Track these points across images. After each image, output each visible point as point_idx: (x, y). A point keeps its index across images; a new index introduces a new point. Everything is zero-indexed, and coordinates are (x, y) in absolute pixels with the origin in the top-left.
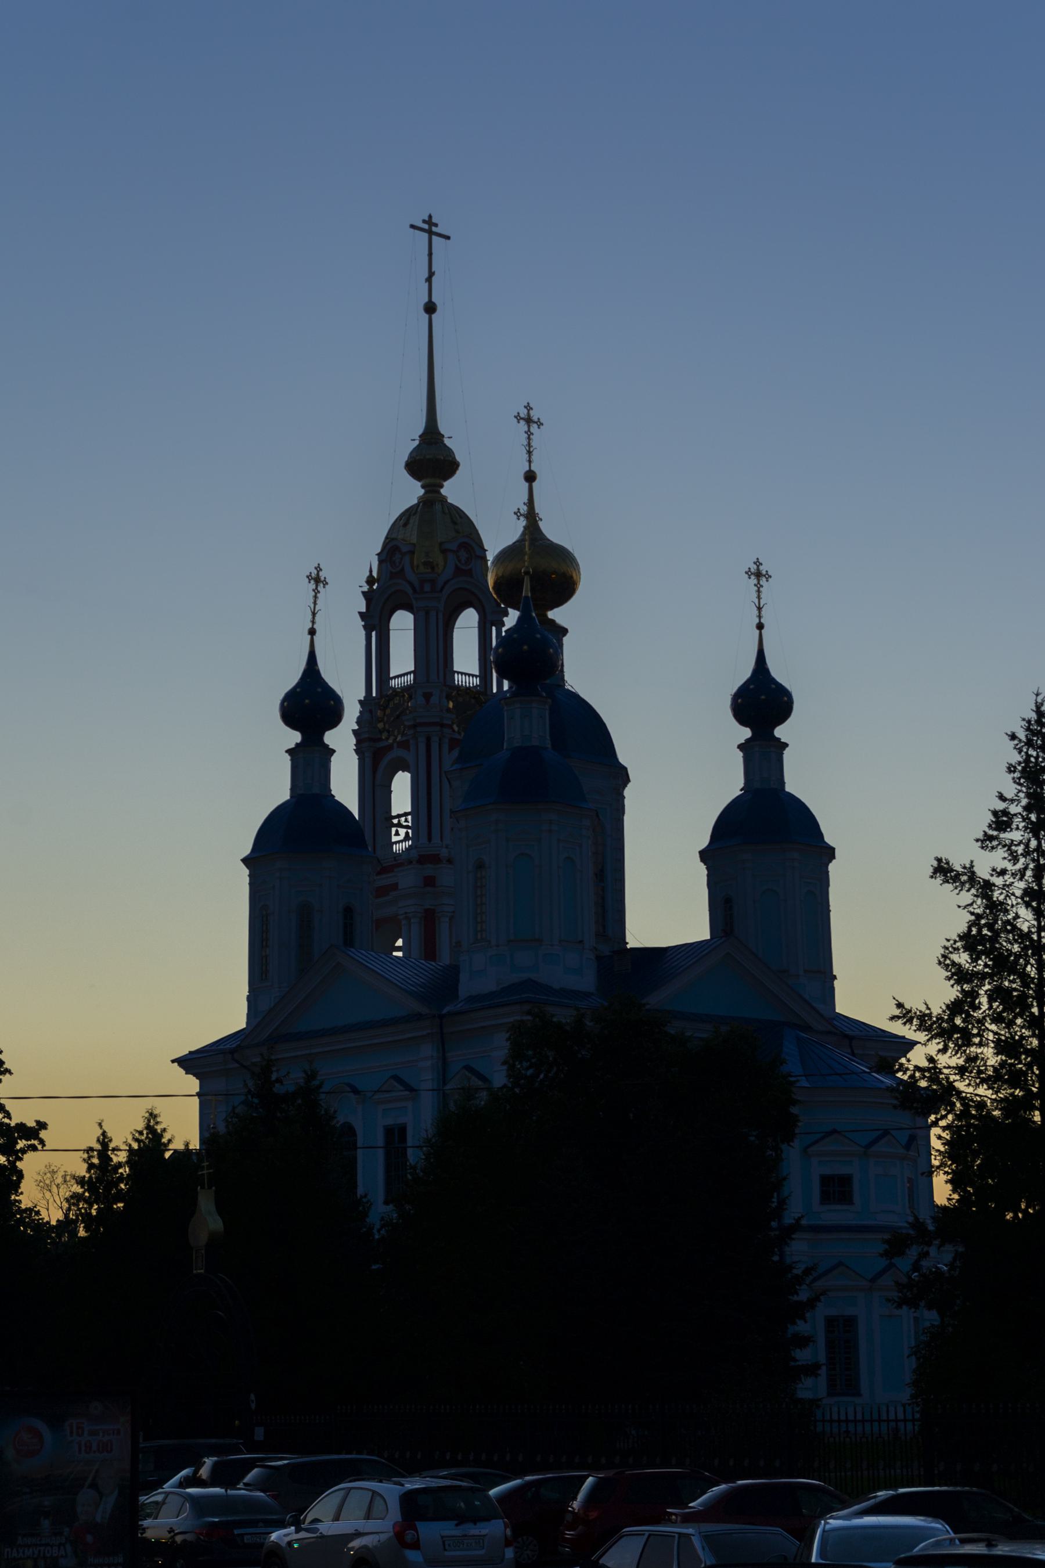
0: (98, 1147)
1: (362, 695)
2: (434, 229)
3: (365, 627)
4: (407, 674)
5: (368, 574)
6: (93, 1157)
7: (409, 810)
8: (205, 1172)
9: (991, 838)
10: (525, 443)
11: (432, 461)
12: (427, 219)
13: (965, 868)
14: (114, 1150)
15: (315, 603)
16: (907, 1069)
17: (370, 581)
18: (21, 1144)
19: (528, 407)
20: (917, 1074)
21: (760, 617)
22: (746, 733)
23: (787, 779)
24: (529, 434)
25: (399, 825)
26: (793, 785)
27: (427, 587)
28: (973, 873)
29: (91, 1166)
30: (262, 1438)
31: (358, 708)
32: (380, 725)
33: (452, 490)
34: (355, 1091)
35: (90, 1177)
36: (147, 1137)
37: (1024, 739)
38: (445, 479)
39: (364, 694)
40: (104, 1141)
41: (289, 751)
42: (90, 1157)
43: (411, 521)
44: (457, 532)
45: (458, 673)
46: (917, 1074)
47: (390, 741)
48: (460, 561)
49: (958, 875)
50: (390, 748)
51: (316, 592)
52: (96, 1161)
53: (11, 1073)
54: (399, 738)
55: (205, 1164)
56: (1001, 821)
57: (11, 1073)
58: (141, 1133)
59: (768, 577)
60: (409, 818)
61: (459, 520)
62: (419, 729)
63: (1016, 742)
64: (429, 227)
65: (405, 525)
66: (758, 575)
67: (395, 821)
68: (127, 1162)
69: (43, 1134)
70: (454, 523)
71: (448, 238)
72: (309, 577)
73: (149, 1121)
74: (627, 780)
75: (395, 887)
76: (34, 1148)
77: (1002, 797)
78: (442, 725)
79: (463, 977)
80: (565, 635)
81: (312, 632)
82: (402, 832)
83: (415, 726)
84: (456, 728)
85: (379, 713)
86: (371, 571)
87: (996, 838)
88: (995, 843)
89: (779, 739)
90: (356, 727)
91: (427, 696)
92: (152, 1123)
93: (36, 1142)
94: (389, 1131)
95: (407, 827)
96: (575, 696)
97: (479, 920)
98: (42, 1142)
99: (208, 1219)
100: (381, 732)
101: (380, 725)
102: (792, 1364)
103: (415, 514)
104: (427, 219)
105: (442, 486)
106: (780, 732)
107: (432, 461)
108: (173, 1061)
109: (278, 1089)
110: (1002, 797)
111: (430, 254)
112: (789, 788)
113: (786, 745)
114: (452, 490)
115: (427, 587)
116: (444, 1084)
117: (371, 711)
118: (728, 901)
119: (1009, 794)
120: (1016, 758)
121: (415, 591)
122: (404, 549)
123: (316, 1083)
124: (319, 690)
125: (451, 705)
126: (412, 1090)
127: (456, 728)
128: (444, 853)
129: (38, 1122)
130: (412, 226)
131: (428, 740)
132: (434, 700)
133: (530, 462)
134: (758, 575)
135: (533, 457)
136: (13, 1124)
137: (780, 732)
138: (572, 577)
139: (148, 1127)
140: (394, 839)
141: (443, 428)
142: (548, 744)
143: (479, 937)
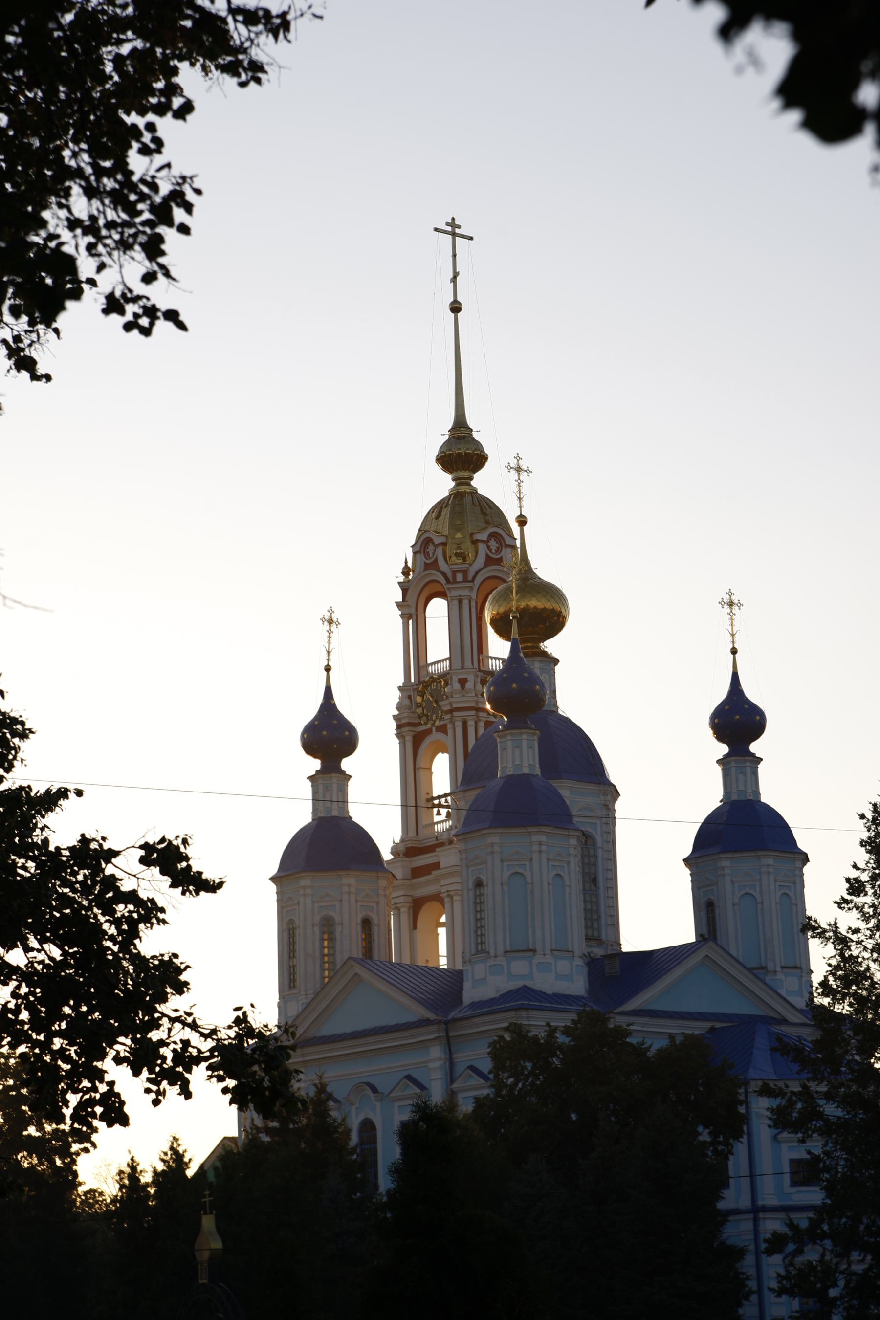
1: (401, 681)
2: (457, 231)
3: (402, 616)
4: (443, 661)
5: (403, 565)
7: (448, 791)
8: (207, 1199)
9: (847, 902)
10: (516, 490)
12: (450, 221)
13: (830, 925)
14: (141, 1171)
16: (785, 1094)
17: (406, 572)
18: (75, 1147)
19: (518, 458)
20: (794, 1098)
22: (724, 749)
23: (762, 790)
24: (519, 482)
25: (440, 806)
27: (459, 577)
28: (837, 928)
32: (419, 711)
33: (483, 482)
34: (374, 1089)
35: (122, 1197)
36: (171, 1158)
37: (870, 818)
38: (475, 472)
39: (403, 681)
40: (133, 1166)
43: (443, 513)
44: (487, 522)
45: (492, 658)
46: (794, 1098)
47: (429, 726)
48: (490, 550)
49: (825, 931)
50: (428, 732)
51: (330, 632)
54: (437, 723)
55: (207, 1193)
56: (856, 887)
60: (449, 798)
61: (488, 511)
62: (455, 714)
63: (865, 821)
64: (453, 230)
65: (437, 518)
67: (436, 802)
68: (153, 1182)
70: (485, 514)
71: (471, 238)
72: (323, 620)
75: (436, 866)
76: (86, 1150)
77: (855, 866)
79: (467, 985)
80: (556, 664)
81: (328, 669)
83: (451, 711)
85: (419, 699)
86: (406, 562)
87: (851, 901)
88: (851, 906)
89: (753, 755)
90: (396, 713)
91: (463, 682)
93: (88, 1145)
96: (567, 721)
97: (479, 933)
98: (94, 1145)
99: (210, 1238)
100: (420, 717)
101: (419, 711)
103: (446, 507)
104: (450, 221)
105: (472, 479)
110: (855, 866)
111: (454, 256)
112: (764, 799)
114: (483, 482)
115: (459, 577)
116: (452, 1082)
117: (410, 697)
119: (862, 865)
120: (865, 835)
121: (448, 581)
122: (437, 540)
124: (335, 722)
130: (436, 230)
131: (465, 723)
132: (469, 685)
133: (520, 507)
135: (523, 503)
138: (561, 612)
139: (172, 1148)
140: (436, 819)
141: (471, 422)
142: (538, 771)
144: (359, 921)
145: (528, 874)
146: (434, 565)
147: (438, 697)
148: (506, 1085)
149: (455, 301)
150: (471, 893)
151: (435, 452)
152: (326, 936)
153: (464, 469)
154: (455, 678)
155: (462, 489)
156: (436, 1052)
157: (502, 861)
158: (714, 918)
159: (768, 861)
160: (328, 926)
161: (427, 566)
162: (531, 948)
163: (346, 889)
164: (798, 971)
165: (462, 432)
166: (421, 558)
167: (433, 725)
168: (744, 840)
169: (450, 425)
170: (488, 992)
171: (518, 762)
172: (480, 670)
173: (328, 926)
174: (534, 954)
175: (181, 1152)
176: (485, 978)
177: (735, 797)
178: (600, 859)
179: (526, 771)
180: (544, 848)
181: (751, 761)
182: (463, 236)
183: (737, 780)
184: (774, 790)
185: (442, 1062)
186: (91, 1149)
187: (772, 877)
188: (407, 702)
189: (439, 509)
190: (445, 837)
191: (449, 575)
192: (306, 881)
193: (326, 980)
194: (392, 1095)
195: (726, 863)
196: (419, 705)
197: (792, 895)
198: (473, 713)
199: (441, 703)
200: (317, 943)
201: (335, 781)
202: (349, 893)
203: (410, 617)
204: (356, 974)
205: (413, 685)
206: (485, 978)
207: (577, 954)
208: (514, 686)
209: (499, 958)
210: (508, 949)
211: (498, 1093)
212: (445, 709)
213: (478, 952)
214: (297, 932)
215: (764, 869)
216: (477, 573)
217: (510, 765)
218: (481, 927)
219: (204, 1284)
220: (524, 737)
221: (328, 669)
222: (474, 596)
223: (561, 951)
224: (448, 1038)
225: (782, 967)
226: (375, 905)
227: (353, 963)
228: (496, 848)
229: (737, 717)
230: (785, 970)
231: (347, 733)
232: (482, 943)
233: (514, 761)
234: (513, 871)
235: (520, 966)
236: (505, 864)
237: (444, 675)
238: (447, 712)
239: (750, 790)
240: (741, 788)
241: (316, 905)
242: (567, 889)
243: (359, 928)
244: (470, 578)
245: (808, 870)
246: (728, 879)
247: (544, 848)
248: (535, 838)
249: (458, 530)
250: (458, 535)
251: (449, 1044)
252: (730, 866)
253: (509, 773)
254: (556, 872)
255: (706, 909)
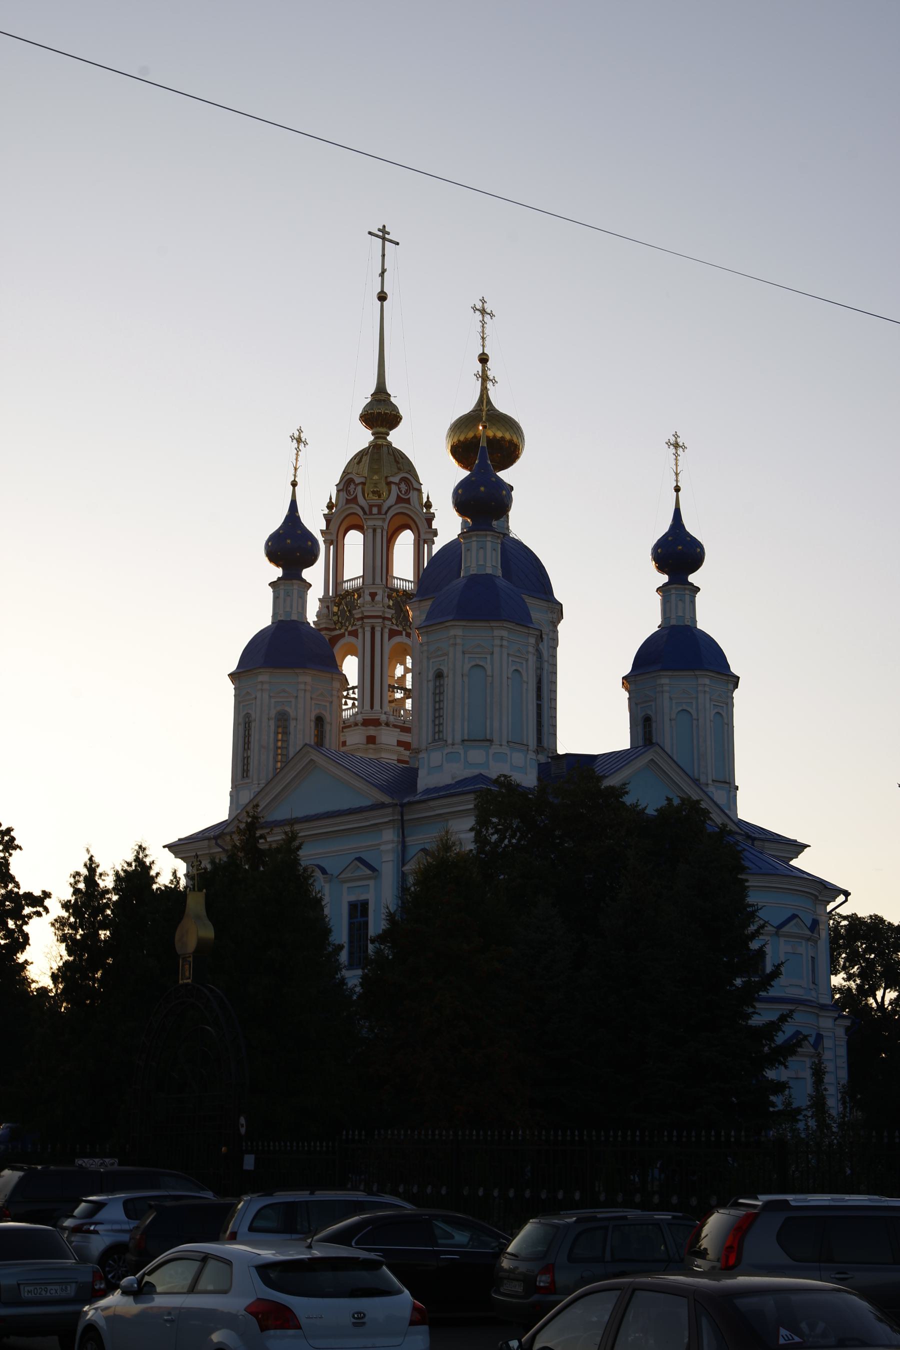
0: (84, 872)
2: (387, 236)
4: (357, 578)
6: (79, 881)
7: (356, 684)
10: (480, 330)
11: (381, 414)
14: (101, 875)
15: (297, 460)
17: (330, 506)
18: (27, 910)
19: (483, 301)
21: (677, 481)
24: (483, 323)
26: (703, 624)
27: (375, 510)
29: (76, 891)
30: (252, 1168)
31: (318, 604)
32: (335, 618)
33: (397, 438)
38: (391, 430)
40: (92, 866)
41: (272, 584)
42: (76, 882)
44: (399, 469)
45: (397, 578)
47: (343, 631)
48: (401, 492)
50: (343, 635)
51: (298, 450)
52: (82, 886)
53: (21, 848)
57: (21, 848)
58: (129, 864)
59: (684, 448)
60: (356, 690)
61: (401, 462)
62: (365, 621)
64: (383, 235)
65: (359, 463)
66: (676, 445)
69: (47, 902)
70: (398, 462)
71: (398, 244)
73: (138, 853)
74: (560, 616)
76: (39, 914)
78: (384, 618)
79: (422, 773)
81: (294, 484)
82: (350, 702)
83: (362, 619)
84: (394, 622)
85: (335, 609)
86: (331, 499)
89: (692, 584)
91: (373, 595)
92: (141, 856)
93: (41, 909)
94: (353, 906)
95: (354, 699)
97: (437, 723)
98: (46, 910)
100: (335, 624)
101: (335, 618)
102: (771, 1109)
105: (388, 435)
106: (692, 578)
107: (381, 414)
108: (164, 847)
109: (262, 845)
111: (383, 255)
112: (699, 626)
113: (698, 589)
114: (397, 438)
115: (375, 510)
116: (403, 865)
117: (328, 607)
118: (647, 720)
121: (365, 513)
122: (358, 480)
123: (296, 843)
124: (299, 532)
125: (391, 603)
126: (373, 869)
127: (394, 622)
128: (383, 718)
129: (44, 892)
130: (370, 233)
132: (378, 598)
133: (483, 346)
134: (676, 445)
135: (486, 343)
136: (21, 892)
137: (692, 578)
139: (137, 859)
142: (499, 573)
143: (437, 737)
144: (313, 718)
145: (488, 667)
146: (354, 500)
147: (352, 606)
148: (489, 843)
149: (382, 292)
150: (431, 685)
151: (360, 411)
152: (280, 730)
153: (382, 426)
154: (367, 592)
155: (380, 442)
156: (389, 835)
157: (464, 653)
158: (650, 732)
159: (705, 680)
160: (283, 721)
161: (348, 501)
162: (488, 738)
163: (302, 686)
164: (727, 786)
165: (383, 397)
166: (344, 495)
167: (346, 630)
168: (680, 667)
169: (372, 390)
170: (444, 779)
171: (481, 563)
172: (387, 587)
173: (283, 721)
174: (491, 745)
175: (148, 864)
176: (441, 766)
177: (673, 622)
178: (545, 672)
179: (489, 571)
180: (505, 643)
181: (690, 590)
182: (391, 241)
183: (677, 606)
184: (709, 619)
185: (395, 845)
186: (44, 913)
187: (708, 696)
188: (325, 611)
189: (360, 457)
190: (352, 720)
191: (367, 509)
192: (264, 677)
193: (279, 765)
194: (342, 876)
195: (665, 681)
196: (335, 614)
197: (724, 714)
198: (380, 620)
199: (354, 612)
200: (272, 735)
201: (295, 587)
202: (305, 690)
203: (331, 543)
204: (312, 760)
205: (331, 597)
206: (441, 766)
207: (531, 748)
208: (482, 489)
209: (456, 746)
210: (466, 738)
211: (480, 850)
212: (356, 616)
213: (434, 740)
214: (253, 725)
215: (700, 688)
216: (389, 508)
217: (474, 565)
218: (440, 716)
219: (187, 985)
220: (489, 539)
221: (294, 484)
222: (386, 527)
223: (516, 744)
224: (402, 820)
225: (713, 781)
226: (328, 704)
227: (310, 749)
228: (459, 641)
229: (680, 548)
230: (717, 784)
231: (310, 543)
232: (439, 732)
233: (477, 561)
234: (474, 663)
235: (476, 755)
236: (467, 656)
237: (357, 590)
238: (358, 619)
239: (687, 616)
240: (680, 614)
241: (273, 700)
242: (525, 685)
243: (313, 724)
244: (383, 511)
245: (738, 695)
246: (666, 695)
247: (505, 643)
248: (497, 633)
249: (376, 473)
250: (376, 477)
251: (402, 827)
252: (671, 685)
253: (472, 573)
254: (515, 668)
255: (643, 724)
